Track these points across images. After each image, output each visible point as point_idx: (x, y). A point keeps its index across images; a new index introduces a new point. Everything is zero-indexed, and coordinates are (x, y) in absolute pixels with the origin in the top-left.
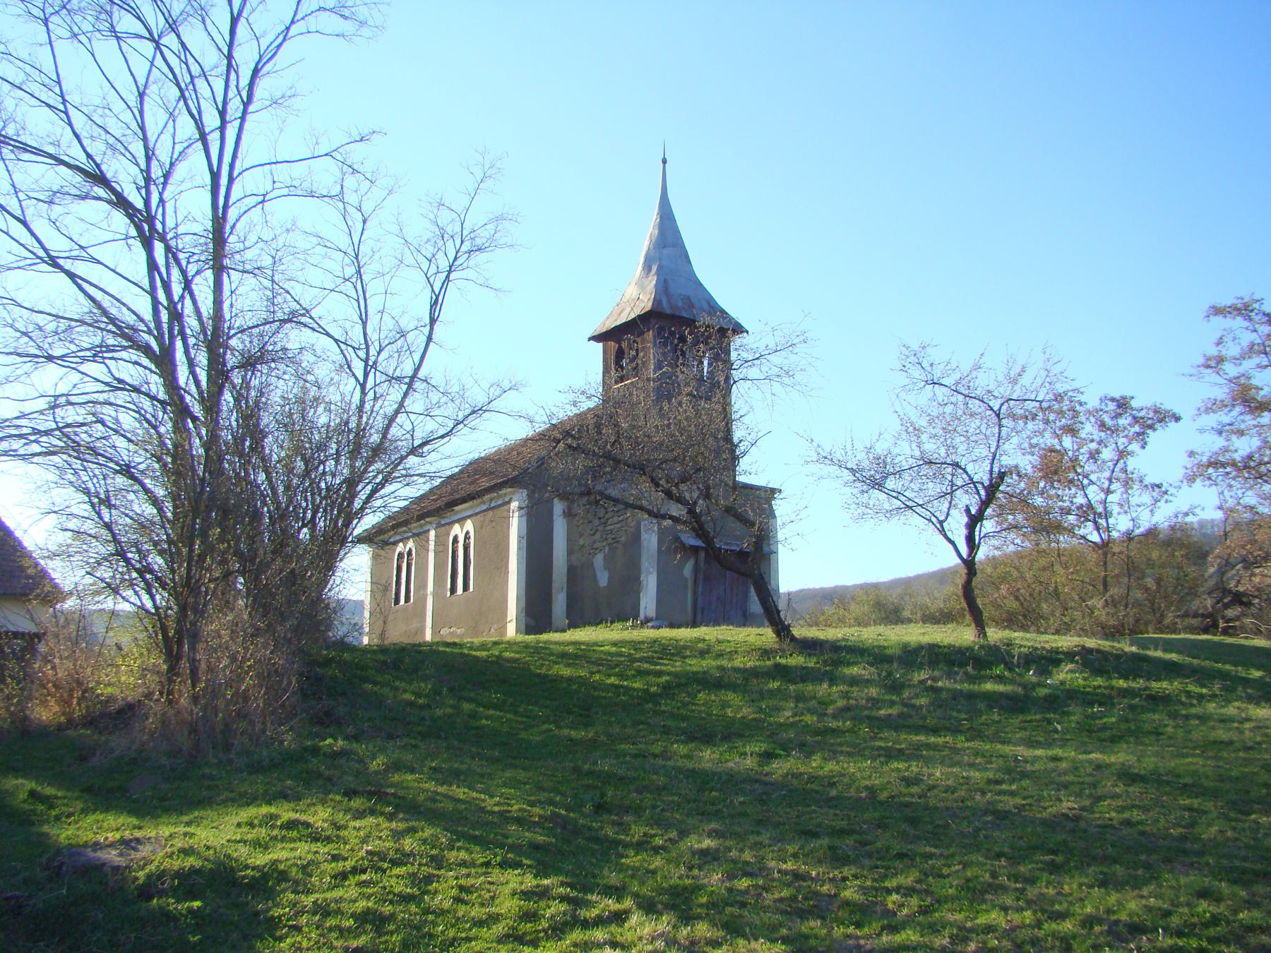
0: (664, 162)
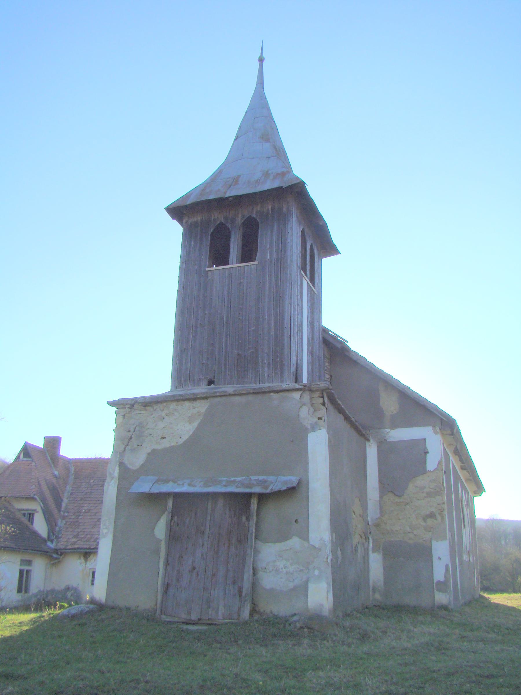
0: (261, 60)
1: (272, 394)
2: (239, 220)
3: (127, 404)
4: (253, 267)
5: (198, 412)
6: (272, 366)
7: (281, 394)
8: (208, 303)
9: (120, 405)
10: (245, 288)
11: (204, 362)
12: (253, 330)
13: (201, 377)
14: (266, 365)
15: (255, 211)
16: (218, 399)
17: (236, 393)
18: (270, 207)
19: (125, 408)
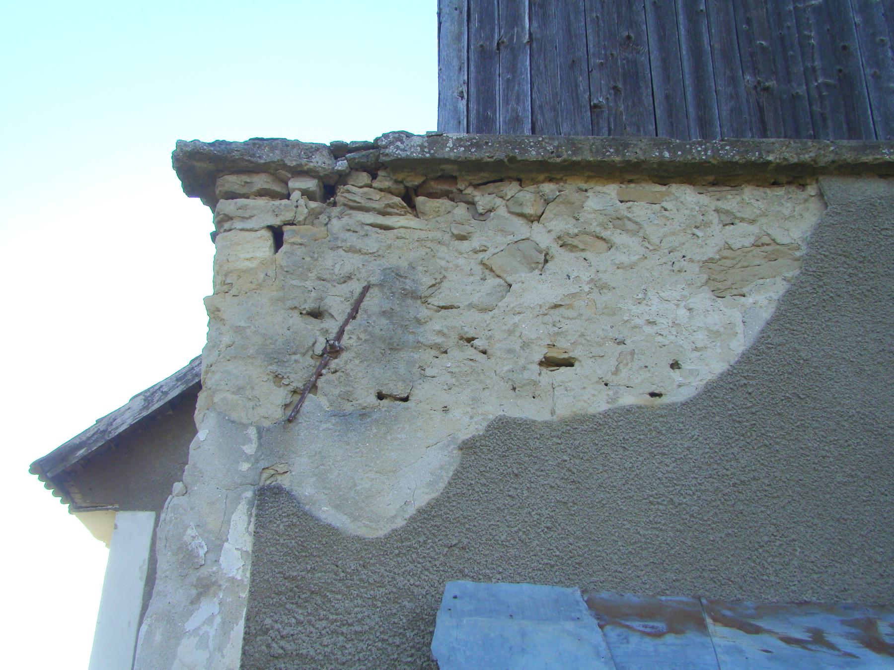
3: (300, 172)
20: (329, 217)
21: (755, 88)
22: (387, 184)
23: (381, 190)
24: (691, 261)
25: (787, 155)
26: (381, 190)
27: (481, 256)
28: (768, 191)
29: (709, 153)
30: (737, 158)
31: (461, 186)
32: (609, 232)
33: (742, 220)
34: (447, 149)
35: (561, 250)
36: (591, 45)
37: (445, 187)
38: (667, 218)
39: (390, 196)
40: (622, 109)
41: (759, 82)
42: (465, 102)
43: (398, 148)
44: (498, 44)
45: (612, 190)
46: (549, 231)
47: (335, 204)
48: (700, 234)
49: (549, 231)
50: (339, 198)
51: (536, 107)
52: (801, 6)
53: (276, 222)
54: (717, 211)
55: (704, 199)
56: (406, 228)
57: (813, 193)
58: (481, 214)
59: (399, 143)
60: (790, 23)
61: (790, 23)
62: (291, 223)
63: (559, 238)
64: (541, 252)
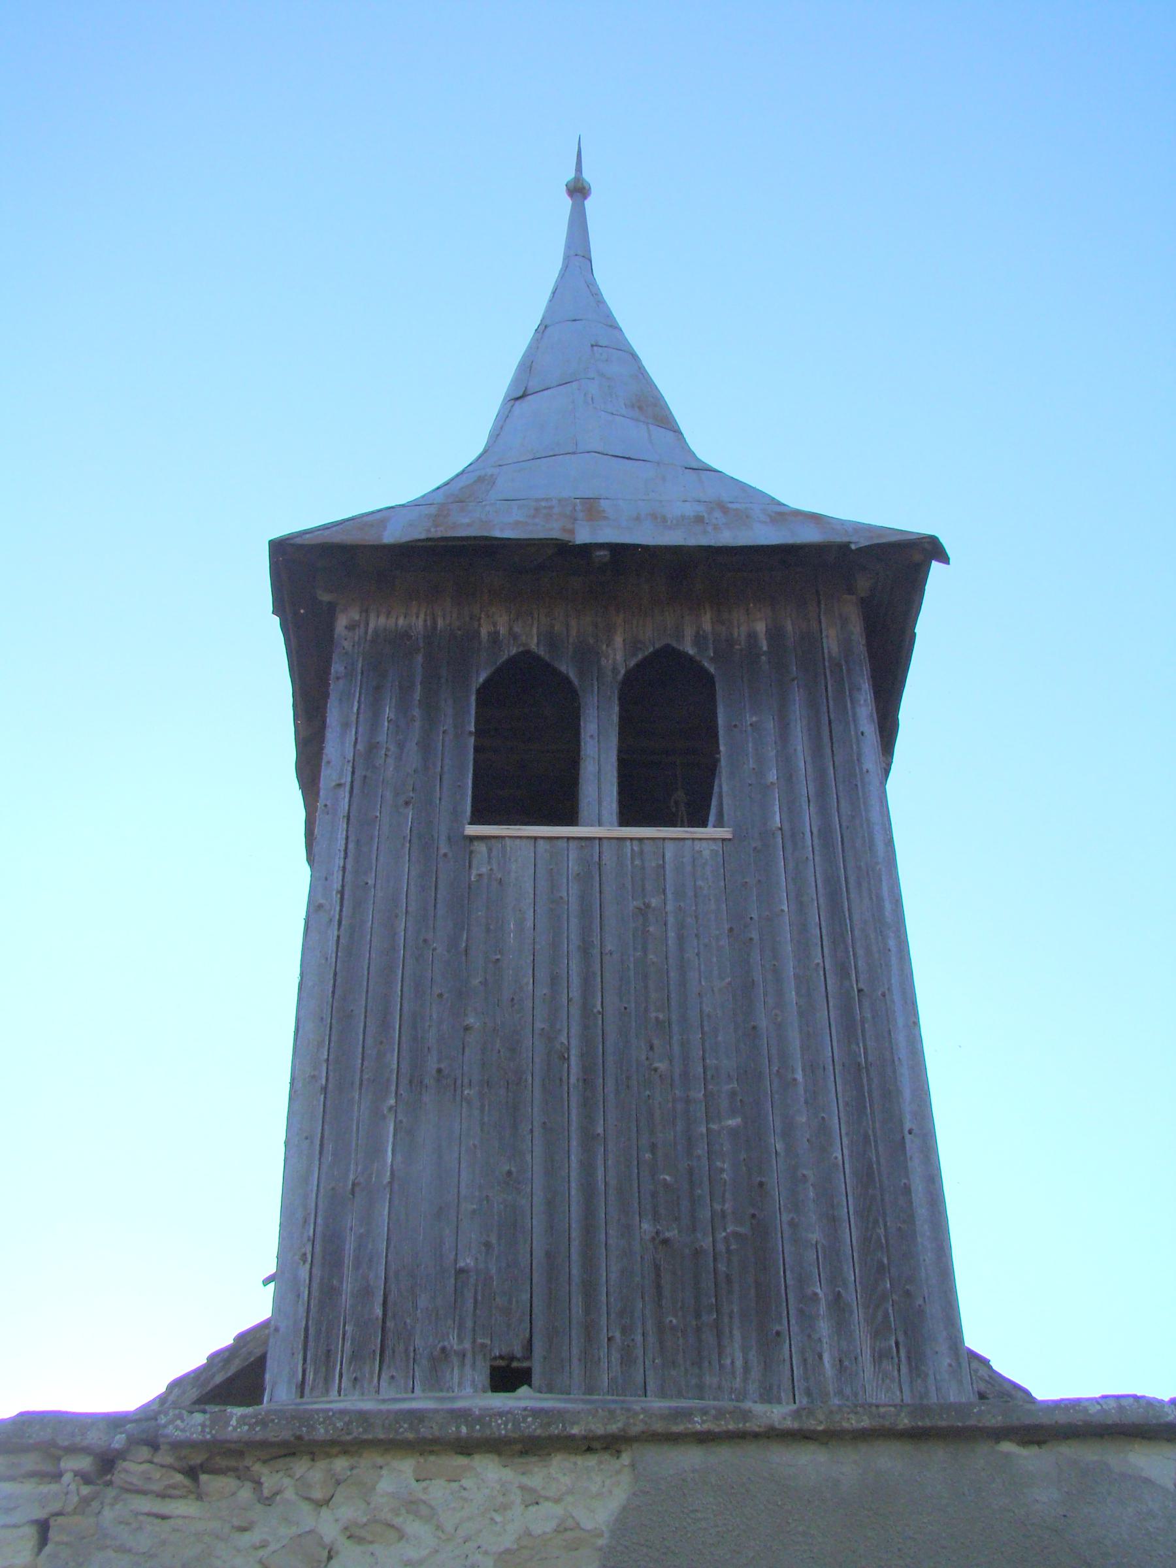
0: (578, 190)
1: (1007, 1447)
2: (617, 656)
3: (72, 1450)
4: (706, 850)
5: (560, 1529)
6: (858, 1316)
7: (1068, 1450)
8: (476, 982)
9: (25, 1449)
10: (671, 934)
11: (467, 1261)
12: (734, 1133)
13: (453, 1342)
14: (823, 1308)
15: (692, 633)
16: (691, 1458)
17: (811, 1424)
18: (761, 627)
19: (57, 1476)
20: (102, 1503)
21: (653, 1239)
22: (169, 1460)
23: (162, 1466)
24: (486, 1553)
25: (593, 1427)
26: (162, 1466)
27: (261, 1553)
28: (579, 1460)
29: (510, 1426)
30: (539, 1432)
31: (248, 1462)
32: (401, 1519)
33: (547, 1499)
34: (230, 1428)
35: (347, 1543)
36: (463, 1184)
37: (233, 1463)
38: (465, 1499)
39: (173, 1473)
40: (494, 1271)
41: (657, 1233)
42: (308, 1266)
43: (177, 1428)
44: (354, 1185)
45: (406, 1467)
46: (337, 1520)
47: (109, 1484)
48: (498, 1518)
49: (337, 1520)
50: (118, 1477)
51: (391, 1274)
52: (714, 1127)
53: (39, 1514)
54: (522, 1488)
55: (508, 1474)
56: (184, 1517)
57: (626, 1463)
58: (267, 1498)
59: (179, 1422)
60: (701, 1150)
61: (701, 1150)
62: (59, 1514)
63: (346, 1528)
64: (324, 1547)
